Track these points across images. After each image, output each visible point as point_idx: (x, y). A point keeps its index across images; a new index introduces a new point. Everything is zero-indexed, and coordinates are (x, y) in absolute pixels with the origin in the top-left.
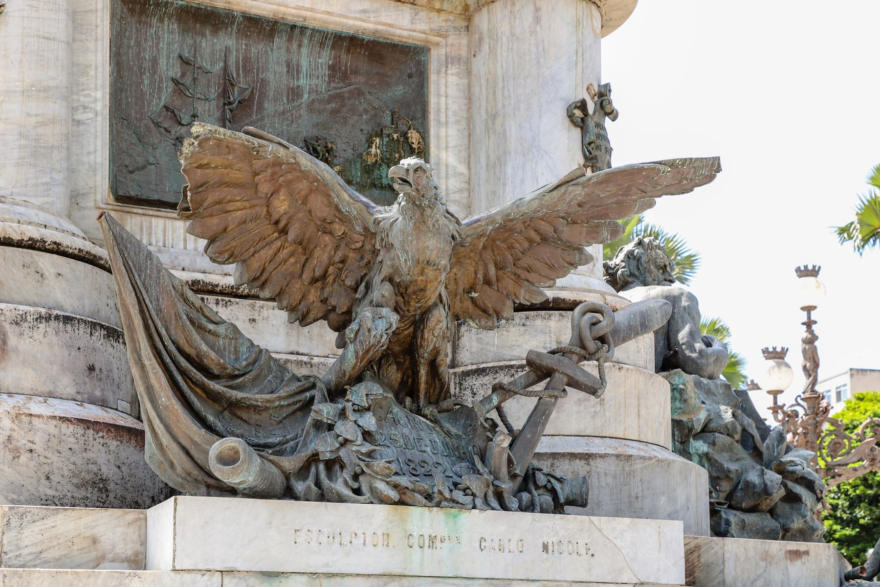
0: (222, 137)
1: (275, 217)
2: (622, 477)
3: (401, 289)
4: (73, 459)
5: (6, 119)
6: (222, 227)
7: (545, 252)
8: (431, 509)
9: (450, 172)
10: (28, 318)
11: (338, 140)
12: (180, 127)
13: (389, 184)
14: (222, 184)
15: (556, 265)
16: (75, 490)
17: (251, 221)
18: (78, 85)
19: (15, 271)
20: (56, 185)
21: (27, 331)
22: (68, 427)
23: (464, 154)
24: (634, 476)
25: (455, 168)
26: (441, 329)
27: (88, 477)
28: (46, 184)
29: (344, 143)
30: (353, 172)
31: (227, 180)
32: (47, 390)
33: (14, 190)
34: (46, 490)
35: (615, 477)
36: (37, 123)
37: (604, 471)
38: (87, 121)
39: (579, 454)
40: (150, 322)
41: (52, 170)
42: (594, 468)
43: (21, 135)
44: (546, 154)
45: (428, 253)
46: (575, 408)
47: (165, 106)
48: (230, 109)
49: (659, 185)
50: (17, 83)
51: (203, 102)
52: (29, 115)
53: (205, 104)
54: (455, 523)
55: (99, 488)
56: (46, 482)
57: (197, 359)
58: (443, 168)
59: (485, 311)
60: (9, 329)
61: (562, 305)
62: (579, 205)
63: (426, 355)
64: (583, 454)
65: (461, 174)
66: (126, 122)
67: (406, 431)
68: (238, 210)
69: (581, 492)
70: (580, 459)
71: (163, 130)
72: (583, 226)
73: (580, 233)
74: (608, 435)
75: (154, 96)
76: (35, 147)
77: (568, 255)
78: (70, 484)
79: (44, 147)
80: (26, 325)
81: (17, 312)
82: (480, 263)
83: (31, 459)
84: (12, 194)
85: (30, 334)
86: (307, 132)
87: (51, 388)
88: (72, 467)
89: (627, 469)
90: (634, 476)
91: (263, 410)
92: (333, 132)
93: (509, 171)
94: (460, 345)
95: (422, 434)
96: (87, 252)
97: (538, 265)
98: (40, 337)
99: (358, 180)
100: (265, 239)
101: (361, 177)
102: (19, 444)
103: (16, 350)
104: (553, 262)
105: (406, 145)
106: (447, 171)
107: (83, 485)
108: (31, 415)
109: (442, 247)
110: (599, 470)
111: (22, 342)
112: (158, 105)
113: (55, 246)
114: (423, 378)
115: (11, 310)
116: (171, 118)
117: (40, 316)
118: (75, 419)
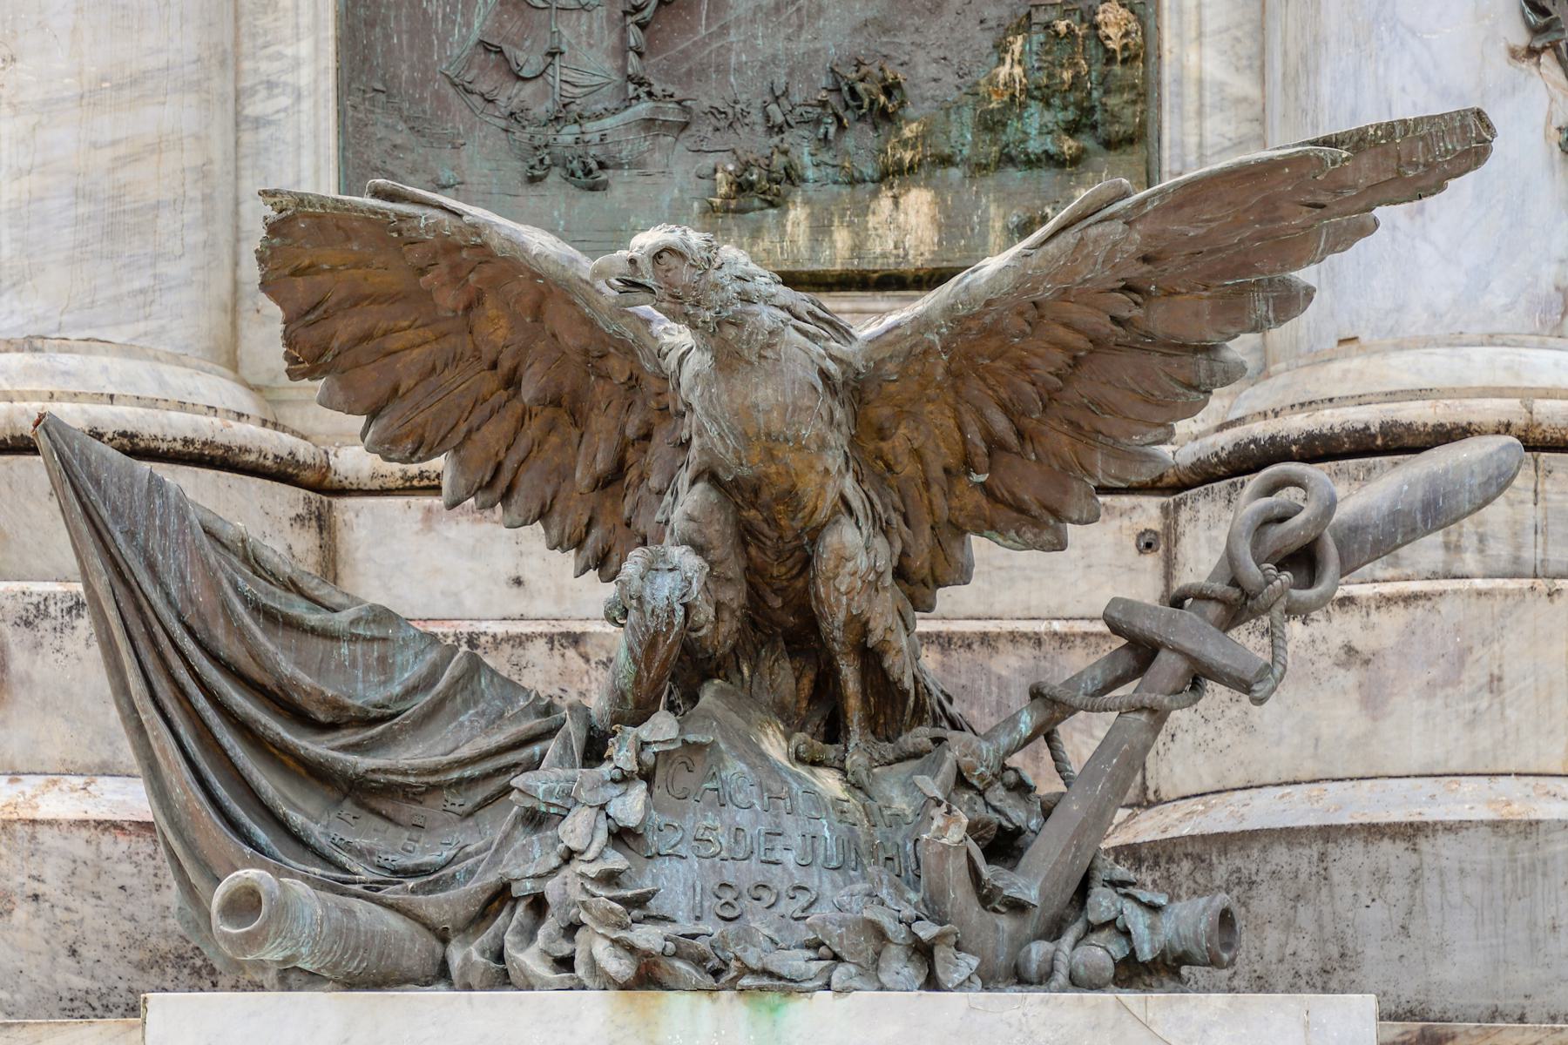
0: (319, 210)
1: (488, 355)
2: (1509, 877)
3: (747, 495)
4: (128, 909)
5: (44, 164)
6: (386, 387)
7: (1125, 367)
8: (715, 994)
9: (1208, 100)
10: (52, 609)
11: (920, 56)
12: (519, 84)
13: (1046, 152)
14: (357, 301)
15: (1157, 393)
16: (135, 974)
17: (446, 365)
18: (254, 36)
19: (32, 507)
20: (170, 288)
21: (50, 637)
22: (116, 842)
23: (1248, 47)
24: (1545, 875)
25: (1221, 86)
26: (854, 574)
27: (164, 946)
28: (142, 291)
29: (936, 61)
30: (954, 133)
31: (367, 290)
32: (97, 760)
33: (65, 318)
34: (71, 979)
35: (1488, 878)
36: (116, 159)
37: (1457, 866)
38: (276, 117)
39: (1389, 825)
40: (157, 628)
41: (157, 257)
42: (1428, 859)
43: (79, 194)
44: (1414, 34)
45: (762, 419)
46: (1419, 706)
47: (481, 42)
48: (637, 23)
49: (1350, 187)
50: (67, 81)
51: (575, 15)
52: (95, 146)
53: (579, 19)
54: (774, 1023)
55: (193, 967)
56: (71, 962)
57: (280, 693)
58: (1191, 91)
59: (1021, 509)
60: (16, 640)
61: (1408, 441)
62: (1146, 259)
63: (837, 634)
64: (1399, 825)
65: (1240, 101)
66: (382, 97)
67: (743, 818)
68: (413, 347)
69: (1195, 933)
70: (1393, 838)
71: (477, 100)
72: (1201, 298)
73: (1197, 314)
74: (1513, 769)
75: (454, 22)
76: (112, 215)
77: (1181, 367)
78: (123, 963)
79: (134, 211)
80: (47, 624)
81: (27, 600)
82: (962, 409)
83: (37, 915)
84: (60, 328)
85: (57, 643)
86: (838, 46)
87: (106, 754)
88: (127, 926)
89: (1524, 856)
90: (1545, 875)
91: (421, 794)
92: (905, 39)
93: (1326, 90)
94: (1179, 556)
95: (788, 822)
96: (205, 443)
97: (1112, 395)
98: (77, 647)
99: (966, 151)
100: (485, 400)
101: (975, 144)
102: (11, 884)
103: (27, 680)
104: (1146, 385)
105: (1091, 44)
106: (1201, 96)
107: (154, 963)
108: (34, 822)
109: (789, 401)
110: (1444, 863)
111: (39, 662)
112: (464, 39)
113: (125, 441)
114: (851, 685)
115: (14, 597)
116: (497, 66)
117: (77, 603)
118: (132, 823)
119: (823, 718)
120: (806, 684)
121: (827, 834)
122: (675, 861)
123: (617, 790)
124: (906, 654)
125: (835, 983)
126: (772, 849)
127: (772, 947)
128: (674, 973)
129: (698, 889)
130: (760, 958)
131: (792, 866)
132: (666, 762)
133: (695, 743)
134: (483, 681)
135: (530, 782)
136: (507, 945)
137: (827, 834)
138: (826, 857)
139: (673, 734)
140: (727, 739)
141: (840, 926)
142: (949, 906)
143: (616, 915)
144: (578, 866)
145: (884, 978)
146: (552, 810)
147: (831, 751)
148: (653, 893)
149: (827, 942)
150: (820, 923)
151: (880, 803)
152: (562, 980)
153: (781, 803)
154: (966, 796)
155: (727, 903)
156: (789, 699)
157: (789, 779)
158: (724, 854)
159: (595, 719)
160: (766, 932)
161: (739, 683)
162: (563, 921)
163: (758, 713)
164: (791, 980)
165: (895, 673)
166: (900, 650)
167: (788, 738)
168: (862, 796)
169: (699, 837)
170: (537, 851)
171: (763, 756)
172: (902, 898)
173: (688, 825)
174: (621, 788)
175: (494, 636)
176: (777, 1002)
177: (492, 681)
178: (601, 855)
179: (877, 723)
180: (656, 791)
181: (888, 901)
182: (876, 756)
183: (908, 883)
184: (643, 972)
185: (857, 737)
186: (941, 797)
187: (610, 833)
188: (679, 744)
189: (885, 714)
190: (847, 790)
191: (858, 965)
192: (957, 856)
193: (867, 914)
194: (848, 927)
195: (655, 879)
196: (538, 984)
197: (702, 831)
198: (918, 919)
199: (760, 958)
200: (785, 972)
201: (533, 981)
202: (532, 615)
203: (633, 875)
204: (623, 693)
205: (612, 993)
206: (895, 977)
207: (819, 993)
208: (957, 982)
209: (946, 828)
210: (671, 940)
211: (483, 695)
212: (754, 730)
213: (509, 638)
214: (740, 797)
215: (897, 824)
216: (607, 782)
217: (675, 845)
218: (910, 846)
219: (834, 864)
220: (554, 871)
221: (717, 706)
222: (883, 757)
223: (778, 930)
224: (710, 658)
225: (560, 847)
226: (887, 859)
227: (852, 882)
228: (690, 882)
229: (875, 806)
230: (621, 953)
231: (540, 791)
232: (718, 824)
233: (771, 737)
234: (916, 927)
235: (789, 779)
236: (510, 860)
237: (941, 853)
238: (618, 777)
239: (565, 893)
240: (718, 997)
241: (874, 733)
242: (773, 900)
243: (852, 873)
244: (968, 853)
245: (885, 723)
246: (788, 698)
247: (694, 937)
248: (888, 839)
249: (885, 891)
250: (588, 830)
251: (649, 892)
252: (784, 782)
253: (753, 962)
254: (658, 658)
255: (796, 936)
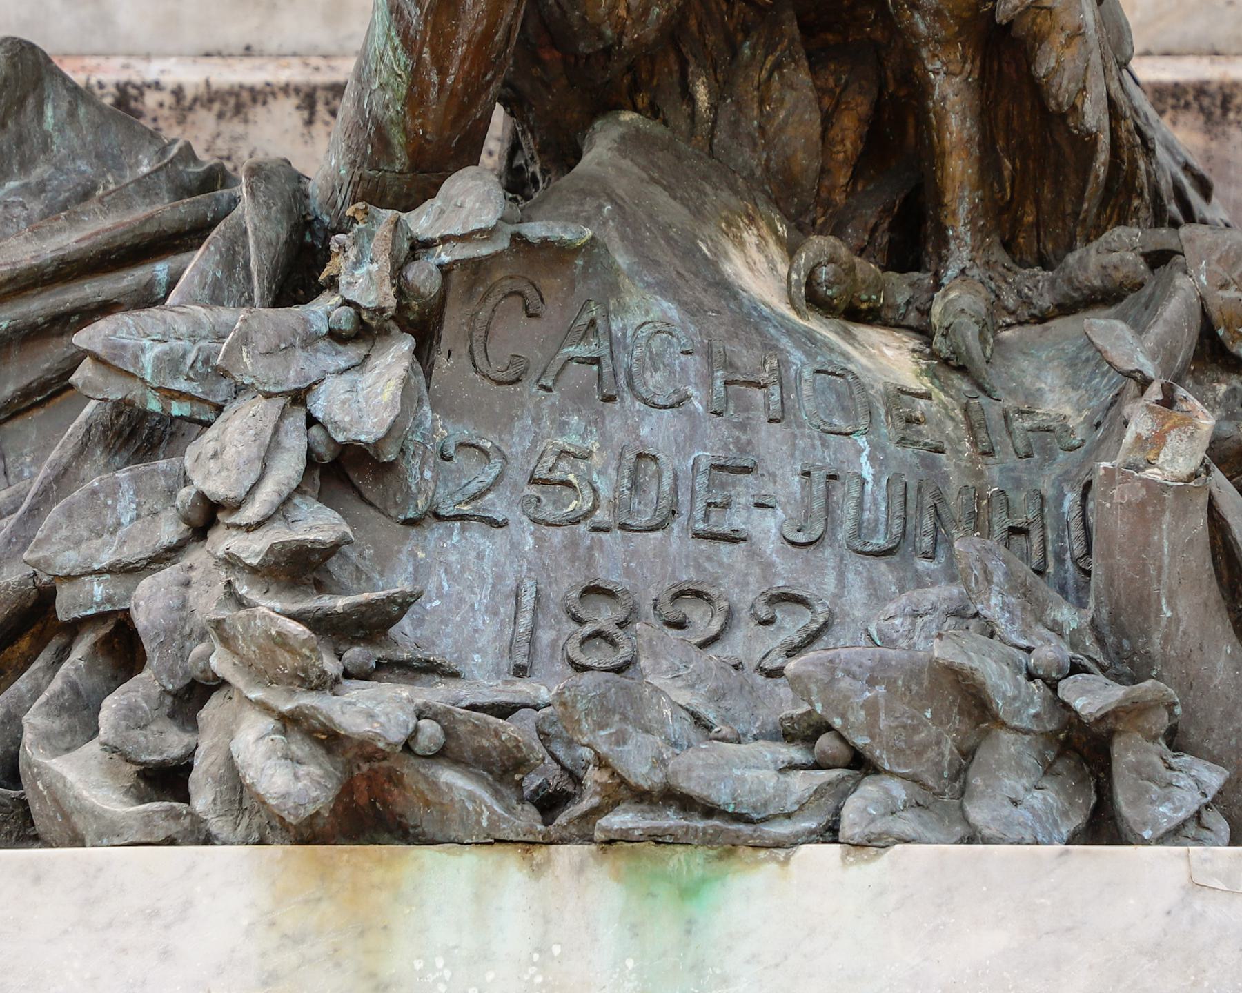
8: (539, 854)
54: (689, 927)
114: (954, 122)
119: (886, 211)
120: (849, 128)
121: (867, 471)
122: (476, 533)
123: (332, 359)
124: (1093, 43)
125: (851, 824)
126: (726, 505)
127: (694, 734)
128: (438, 802)
129: (528, 600)
130: (660, 762)
131: (770, 546)
132: (470, 290)
133: (546, 243)
134: (49, 112)
135: (123, 338)
136: (28, 737)
137: (867, 471)
138: (859, 525)
139: (488, 218)
140: (635, 245)
141: (872, 682)
142: (1157, 639)
143: (293, 651)
144: (224, 541)
145: (978, 814)
146: (177, 409)
147: (900, 288)
148: (405, 603)
149: (837, 722)
150: (820, 674)
151: (1009, 403)
152: (147, 820)
153: (758, 395)
154: (1222, 388)
155: (598, 634)
156: (805, 162)
157: (785, 342)
158: (601, 516)
159: (315, 203)
160: (685, 698)
161: (684, 126)
162: (172, 675)
163: (725, 195)
164: (738, 818)
165: (1063, 89)
166: (1078, 33)
167: (791, 251)
168: (965, 386)
169: (542, 473)
170: (126, 507)
171: (726, 289)
172: (1039, 620)
173: (517, 444)
174: (352, 353)
175: (178, 92)
176: (698, 872)
177: (72, 114)
178: (282, 510)
179: (1016, 222)
180: (442, 362)
181: (1002, 625)
182: (1011, 301)
183: (1063, 590)
184: (362, 798)
185: (965, 253)
186: (1150, 370)
187: (312, 460)
188: (503, 244)
189: (1037, 202)
190: (932, 374)
191: (914, 779)
192: (1182, 513)
193: (943, 651)
194: (890, 684)
195: (420, 571)
196: (89, 831)
197: (550, 460)
198: (1076, 669)
199: (660, 762)
200: (721, 795)
201: (79, 822)
202: (272, 46)
203: (365, 565)
204: (380, 129)
205: (275, 851)
206: (1008, 809)
207: (805, 849)
208: (1165, 825)
209: (1159, 440)
210: (435, 717)
211: (46, 147)
212: (709, 230)
213: (211, 97)
214: (654, 381)
215: (1044, 449)
216: (317, 337)
217: (481, 494)
218: (1071, 499)
219: (880, 542)
220: (171, 553)
221: (620, 170)
222: (1027, 302)
223: (717, 696)
224: (607, 51)
225: (185, 495)
226: (1014, 531)
227: (920, 584)
228: (510, 583)
229: (994, 411)
230: (300, 747)
231: (148, 360)
232: (593, 443)
233: (753, 252)
234: (1069, 690)
235: (785, 342)
236: (56, 527)
237: (1142, 504)
238: (346, 326)
239: (183, 606)
240: (548, 861)
241: (1008, 246)
242: (715, 627)
243: (922, 564)
244: (1212, 507)
245: (1037, 224)
246: (802, 159)
247: (504, 711)
248: (1018, 484)
249: (995, 600)
250: (254, 451)
251: (391, 599)
252: (770, 347)
253: (641, 772)
254: (463, 35)
255: (762, 712)
